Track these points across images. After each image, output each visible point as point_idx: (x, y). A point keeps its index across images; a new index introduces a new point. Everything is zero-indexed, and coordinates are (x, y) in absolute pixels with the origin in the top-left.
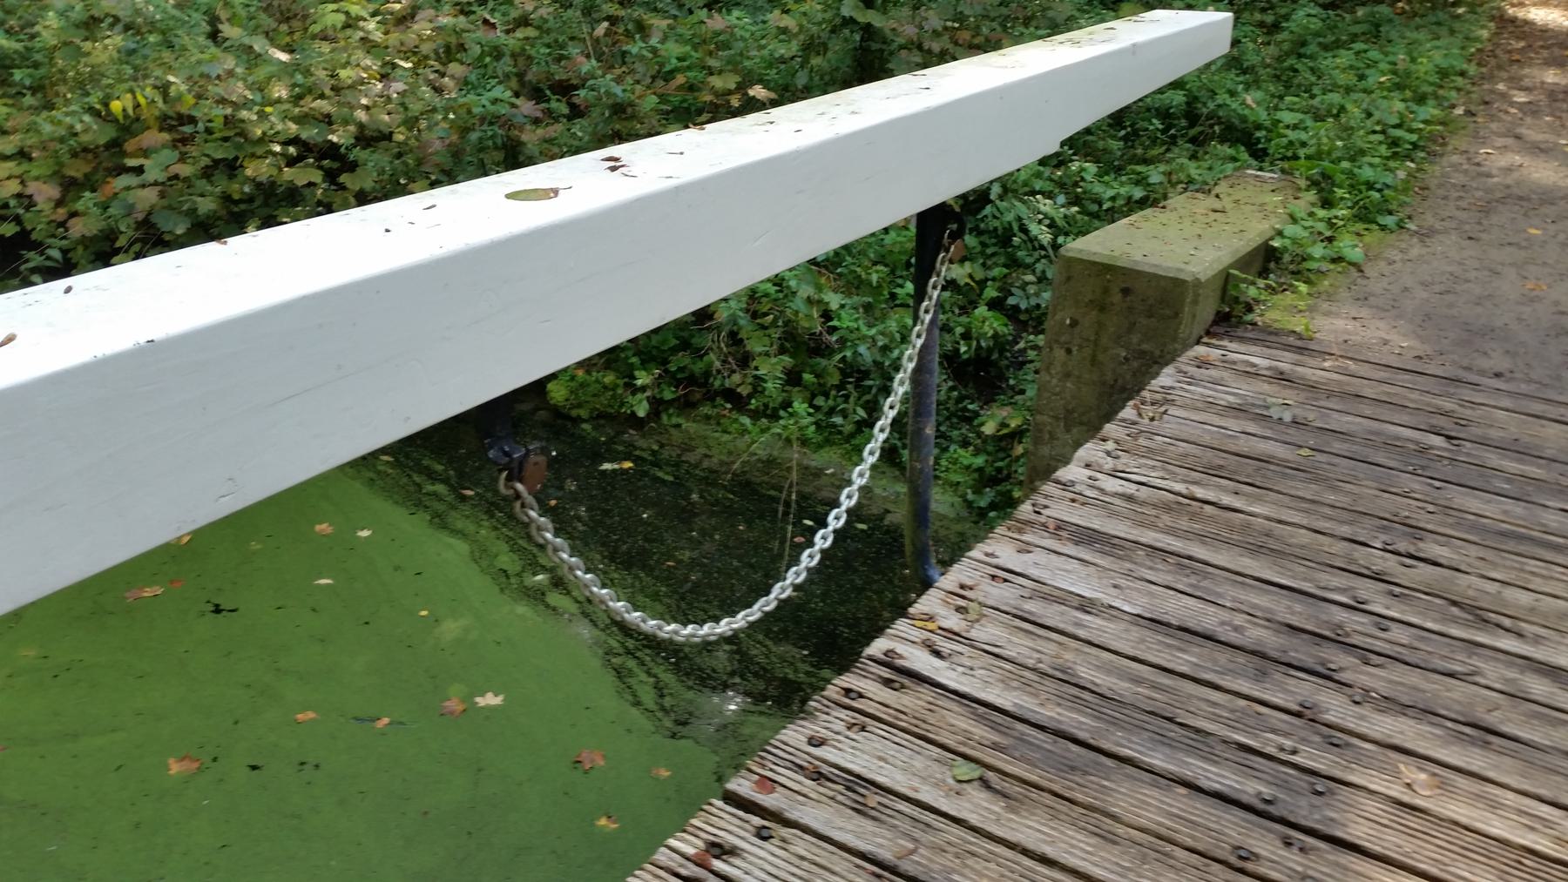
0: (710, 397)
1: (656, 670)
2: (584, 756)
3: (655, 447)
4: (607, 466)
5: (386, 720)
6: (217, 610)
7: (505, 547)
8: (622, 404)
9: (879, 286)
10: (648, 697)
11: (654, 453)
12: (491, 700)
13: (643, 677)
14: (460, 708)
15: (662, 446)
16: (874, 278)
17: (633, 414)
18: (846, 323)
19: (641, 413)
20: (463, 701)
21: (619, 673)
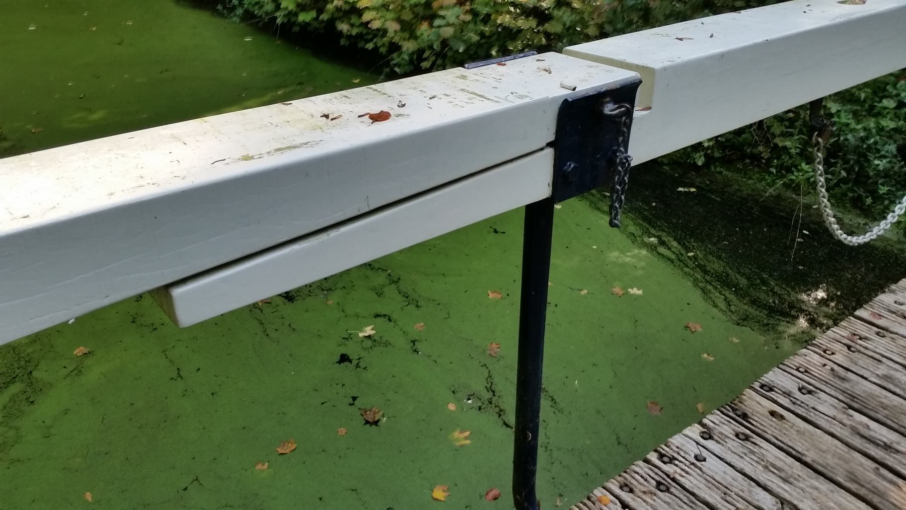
0: (742, 158)
1: (723, 292)
2: (690, 325)
3: (708, 182)
4: (680, 189)
5: (586, 291)
6: (496, 231)
7: (632, 223)
8: (689, 157)
9: (865, 101)
10: (723, 305)
11: (707, 185)
12: (635, 291)
13: (717, 294)
14: (621, 292)
15: (711, 182)
16: (863, 96)
17: (695, 164)
18: (844, 120)
19: (700, 164)
20: (622, 289)
21: (703, 290)
